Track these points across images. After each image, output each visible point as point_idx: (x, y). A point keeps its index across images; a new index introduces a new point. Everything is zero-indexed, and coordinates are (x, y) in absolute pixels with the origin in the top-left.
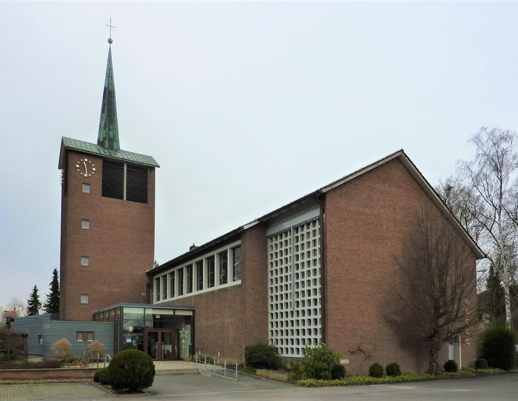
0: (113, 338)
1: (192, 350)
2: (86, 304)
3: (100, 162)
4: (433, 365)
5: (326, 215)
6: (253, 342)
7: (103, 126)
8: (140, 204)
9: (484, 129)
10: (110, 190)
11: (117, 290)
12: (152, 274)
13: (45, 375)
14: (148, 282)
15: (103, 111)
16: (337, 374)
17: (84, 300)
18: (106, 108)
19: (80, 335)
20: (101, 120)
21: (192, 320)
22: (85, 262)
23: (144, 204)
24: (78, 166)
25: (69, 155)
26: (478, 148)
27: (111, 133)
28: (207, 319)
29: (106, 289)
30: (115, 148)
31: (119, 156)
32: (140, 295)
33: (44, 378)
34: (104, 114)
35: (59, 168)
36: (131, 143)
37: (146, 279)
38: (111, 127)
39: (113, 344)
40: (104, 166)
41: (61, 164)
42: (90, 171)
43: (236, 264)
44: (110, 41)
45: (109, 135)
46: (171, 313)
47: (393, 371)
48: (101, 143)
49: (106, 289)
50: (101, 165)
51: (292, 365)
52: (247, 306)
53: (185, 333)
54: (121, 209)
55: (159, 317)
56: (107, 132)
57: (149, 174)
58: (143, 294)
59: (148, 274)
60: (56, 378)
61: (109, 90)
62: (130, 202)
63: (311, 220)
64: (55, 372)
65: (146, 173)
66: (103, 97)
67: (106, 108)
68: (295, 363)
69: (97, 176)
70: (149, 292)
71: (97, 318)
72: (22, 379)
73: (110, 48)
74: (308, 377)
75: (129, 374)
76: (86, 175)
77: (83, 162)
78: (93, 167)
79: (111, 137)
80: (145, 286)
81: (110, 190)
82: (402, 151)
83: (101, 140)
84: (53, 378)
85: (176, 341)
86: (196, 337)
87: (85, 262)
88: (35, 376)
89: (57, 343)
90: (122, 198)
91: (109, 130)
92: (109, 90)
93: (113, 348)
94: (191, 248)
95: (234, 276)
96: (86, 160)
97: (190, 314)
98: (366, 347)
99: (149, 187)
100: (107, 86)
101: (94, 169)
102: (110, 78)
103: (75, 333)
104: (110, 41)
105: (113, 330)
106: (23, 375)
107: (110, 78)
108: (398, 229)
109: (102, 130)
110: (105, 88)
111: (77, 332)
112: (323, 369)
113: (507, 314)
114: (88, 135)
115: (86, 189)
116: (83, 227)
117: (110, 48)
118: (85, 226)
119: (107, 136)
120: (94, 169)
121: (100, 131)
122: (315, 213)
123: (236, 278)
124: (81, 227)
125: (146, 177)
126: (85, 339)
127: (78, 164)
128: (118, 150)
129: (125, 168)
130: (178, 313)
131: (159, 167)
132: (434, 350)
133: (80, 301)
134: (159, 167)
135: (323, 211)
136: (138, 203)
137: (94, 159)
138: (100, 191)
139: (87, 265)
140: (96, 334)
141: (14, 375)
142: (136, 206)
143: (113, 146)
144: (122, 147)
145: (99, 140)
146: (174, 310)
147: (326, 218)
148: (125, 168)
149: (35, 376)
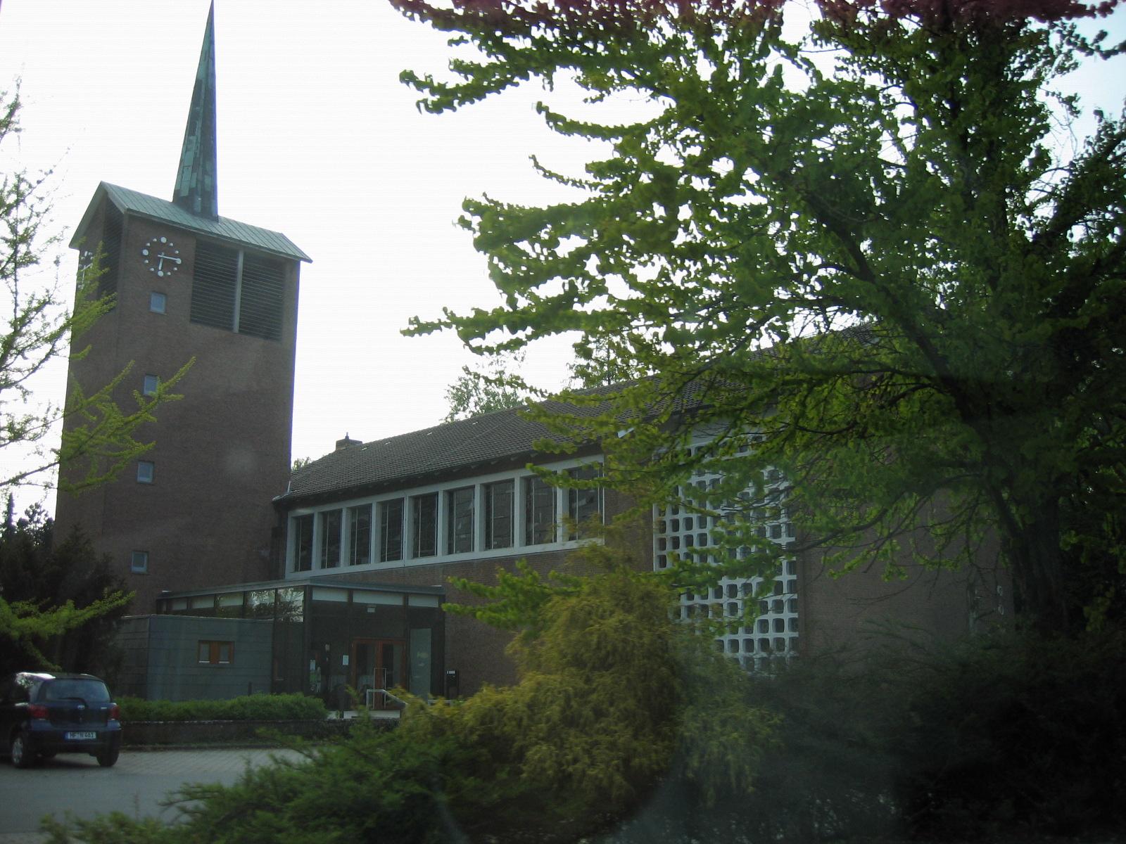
7: (190, 162)
19: (205, 648)
27: (207, 180)
31: (217, 229)
34: (193, 138)
43: (577, 504)
45: (203, 182)
46: (397, 601)
48: (181, 199)
55: (371, 610)
58: (265, 553)
59: (277, 505)
71: (164, 608)
76: (161, 274)
83: (185, 193)
94: (339, 444)
101: (146, 252)
109: (188, 173)
113: (84, 737)
114: (154, 179)
119: (199, 186)
128: (216, 219)
130: (415, 602)
131: (310, 261)
134: (310, 261)
142: (257, 343)
145: (177, 193)
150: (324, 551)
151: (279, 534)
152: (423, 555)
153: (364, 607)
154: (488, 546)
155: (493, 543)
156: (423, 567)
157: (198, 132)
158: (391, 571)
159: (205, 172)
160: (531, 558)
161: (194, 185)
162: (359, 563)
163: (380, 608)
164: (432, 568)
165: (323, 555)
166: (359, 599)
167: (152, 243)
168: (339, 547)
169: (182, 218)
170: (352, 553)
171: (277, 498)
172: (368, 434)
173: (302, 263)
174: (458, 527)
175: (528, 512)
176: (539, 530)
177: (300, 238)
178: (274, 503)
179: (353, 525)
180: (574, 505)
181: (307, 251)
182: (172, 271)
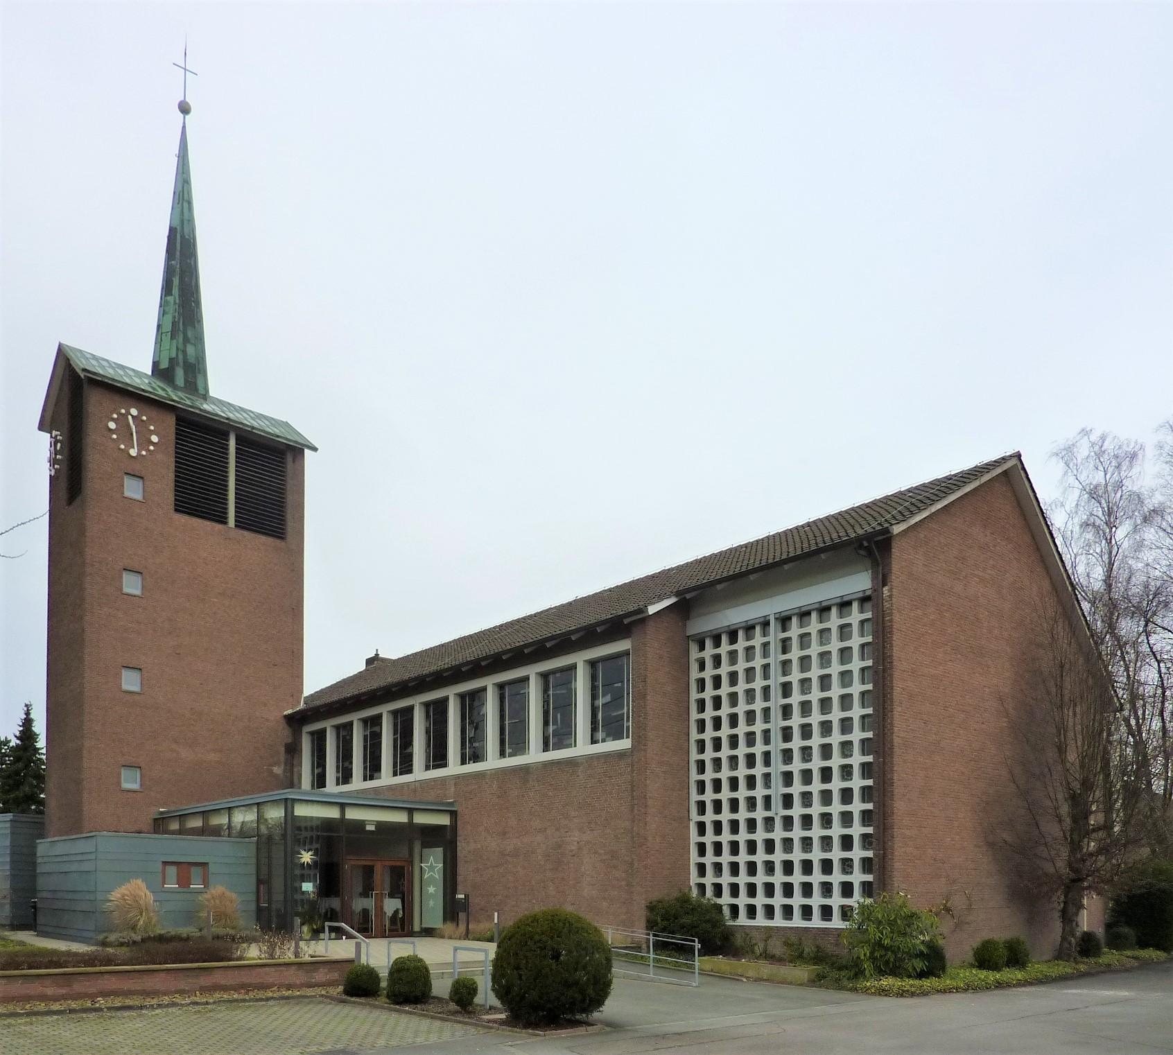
0: (253, 880)
1: (453, 910)
2: (135, 792)
3: (171, 421)
4: (1070, 943)
5: (890, 590)
6: (658, 893)
7: (168, 327)
8: (270, 540)
9: (1085, 432)
10: (196, 496)
11: (213, 757)
12: (296, 721)
13: (205, 981)
14: (290, 741)
15: (167, 288)
16: (932, 963)
17: (130, 781)
18: (176, 281)
19: (172, 870)
20: (163, 311)
21: (448, 836)
22: (130, 682)
23: (278, 541)
24: (112, 425)
25: (77, 394)
26: (1066, 473)
28: (504, 833)
29: (186, 754)
30: (202, 391)
32: (271, 773)
33: (204, 990)
35: (42, 427)
36: (236, 385)
37: (285, 734)
38: (190, 334)
39: (253, 897)
40: (179, 434)
41: (48, 418)
42: (145, 442)
43: (600, 702)
44: (184, 109)
45: (184, 352)
46: (402, 818)
47: (1015, 956)
48: (162, 372)
49: (186, 754)
50: (173, 430)
51: (787, 944)
52: (650, 802)
53: (431, 866)
54: (218, 545)
55: (372, 828)
56: (181, 346)
57: (290, 465)
58: (278, 770)
60: (236, 988)
61: (182, 237)
62: (246, 533)
63: (817, 606)
64: (229, 972)
65: (282, 462)
66: (167, 251)
67: (176, 281)
68: (794, 939)
69: (159, 456)
70: (292, 766)
72: (146, 994)
73: (184, 127)
74: (881, 972)
75: (550, 981)
76: (133, 452)
77: (125, 416)
78: (152, 432)
79: (192, 360)
80: (283, 749)
81: (196, 496)
82: (1018, 456)
84: (224, 989)
85: (401, 884)
86: (460, 878)
87: (130, 682)
88: (182, 985)
89: (116, 895)
90: (222, 520)
91: (186, 340)
92: (182, 237)
93: (253, 907)
94: (369, 662)
95: (594, 729)
96: (134, 412)
97: (445, 820)
98: (958, 902)
99: (290, 498)
100: (176, 223)
101: (155, 439)
102: (186, 205)
103: (159, 866)
104: (184, 109)
105: (254, 861)
106: (149, 983)
107: (186, 205)
108: (1006, 634)
109: (166, 339)
110: (172, 231)
111: (165, 863)
112: (885, 956)
115: (133, 489)
116: (126, 590)
117: (184, 127)
118: (132, 585)
119: (181, 357)
120: (155, 439)
121: (159, 341)
122: (859, 582)
123: (600, 735)
124: (121, 589)
125: (281, 473)
126: (184, 882)
127: (113, 420)
128: (205, 397)
129: (232, 443)
130: (420, 819)
131: (315, 449)
132: (1072, 909)
133: (119, 783)
134: (315, 449)
135: (882, 579)
136: (263, 538)
137: (154, 413)
138: (169, 496)
139: (136, 688)
140: (212, 868)
141: (128, 984)
143: (195, 384)
144: (213, 393)
145: (155, 365)
146: (411, 811)
147: (890, 596)
148: (232, 443)
149: (182, 985)
150: (338, 767)
151: (293, 750)
152: (435, 767)
153: (360, 824)
154: (502, 754)
155: (508, 751)
156: (435, 780)
157: (175, 291)
158: (402, 785)
159: (186, 340)
160: (547, 765)
161: (174, 355)
162: (372, 778)
163: (381, 826)
164: (443, 780)
165: (338, 772)
166: (352, 814)
167: (120, 414)
168: (351, 763)
169: (161, 390)
170: (365, 768)
171: (289, 712)
172: (393, 652)
173: (306, 451)
174: (470, 733)
175: (546, 714)
176: (558, 734)
177: (304, 426)
178: (285, 716)
179: (365, 737)
180: (596, 703)
181: (310, 436)
182: (148, 450)
